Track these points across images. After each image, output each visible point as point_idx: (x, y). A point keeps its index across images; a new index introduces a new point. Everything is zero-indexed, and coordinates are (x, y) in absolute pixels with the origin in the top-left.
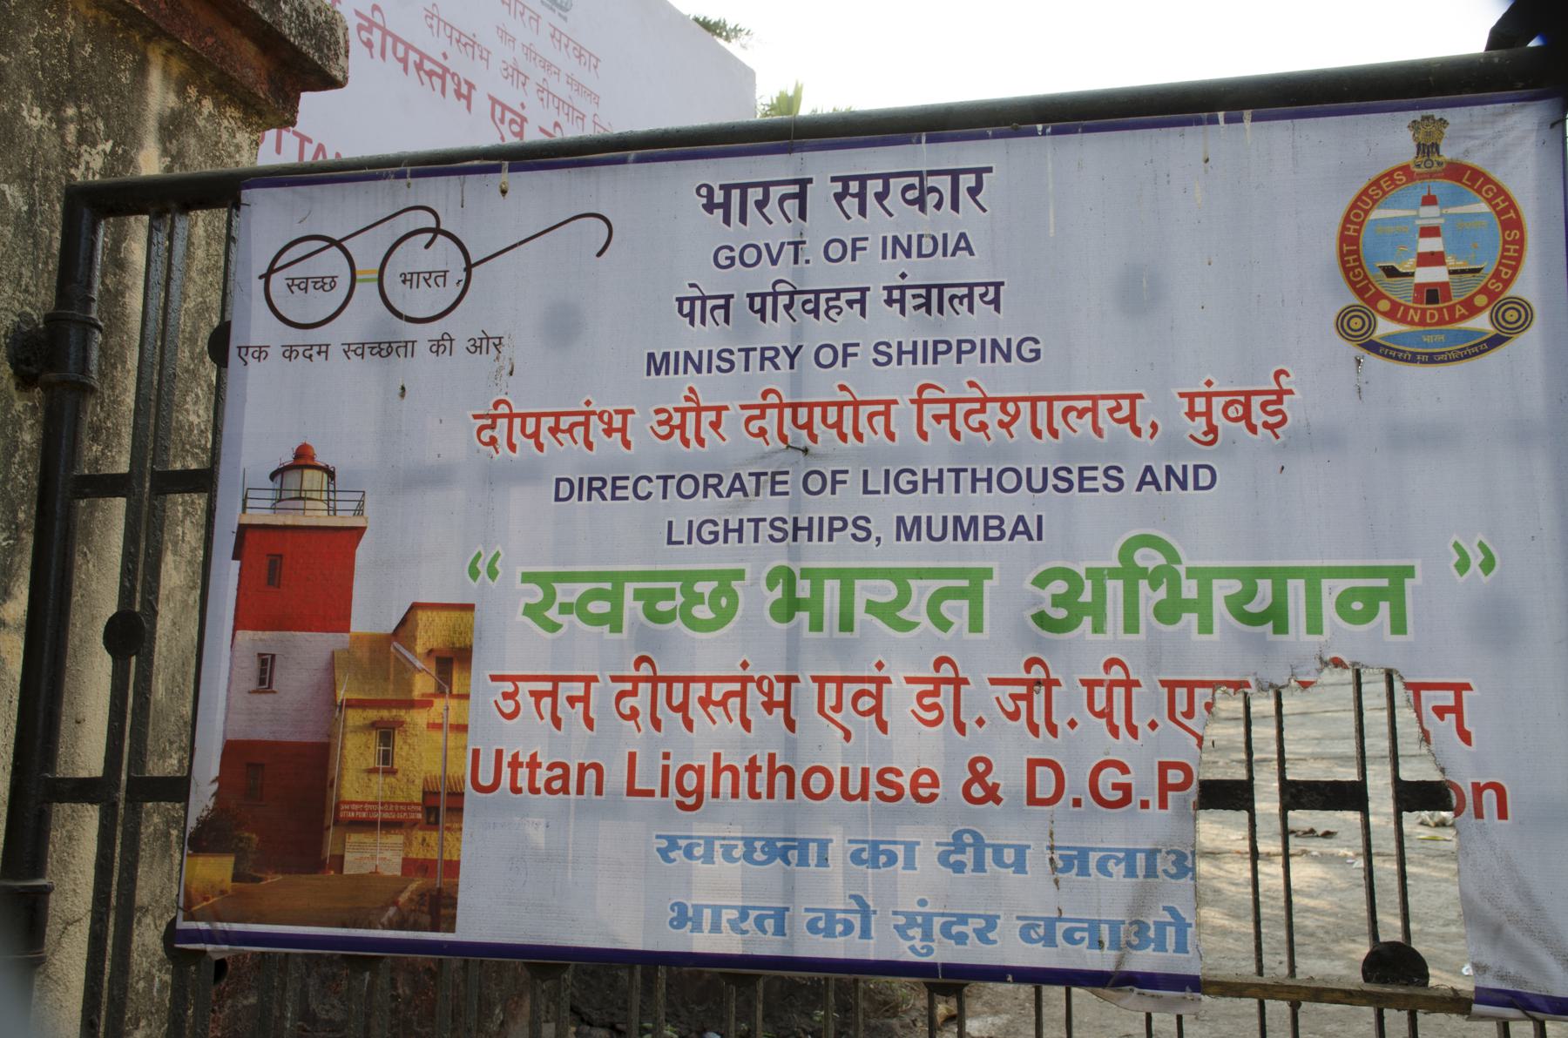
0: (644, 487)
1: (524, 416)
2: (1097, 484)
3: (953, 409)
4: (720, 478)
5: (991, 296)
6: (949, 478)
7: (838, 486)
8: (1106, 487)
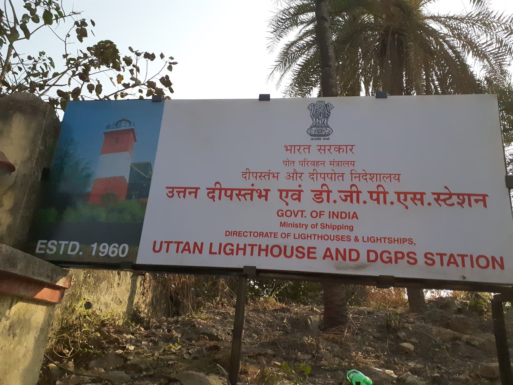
0: (245, 234)
1: (253, 173)
2: (345, 239)
3: (360, 175)
4: (263, 233)
5: (353, 163)
6: (313, 236)
7: (289, 237)
8: (347, 240)
